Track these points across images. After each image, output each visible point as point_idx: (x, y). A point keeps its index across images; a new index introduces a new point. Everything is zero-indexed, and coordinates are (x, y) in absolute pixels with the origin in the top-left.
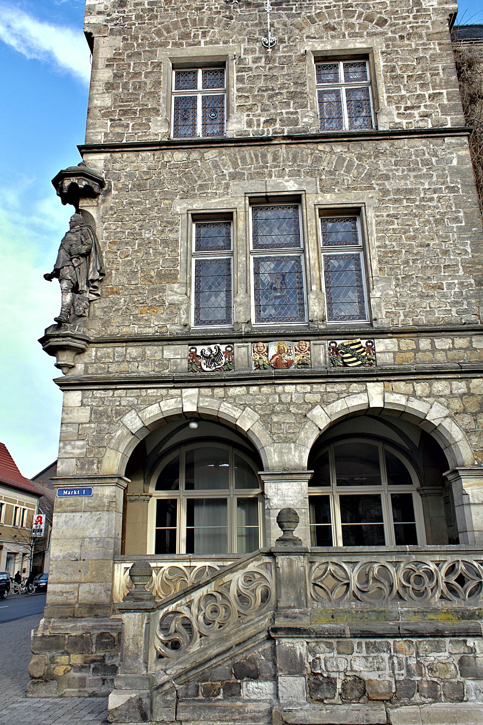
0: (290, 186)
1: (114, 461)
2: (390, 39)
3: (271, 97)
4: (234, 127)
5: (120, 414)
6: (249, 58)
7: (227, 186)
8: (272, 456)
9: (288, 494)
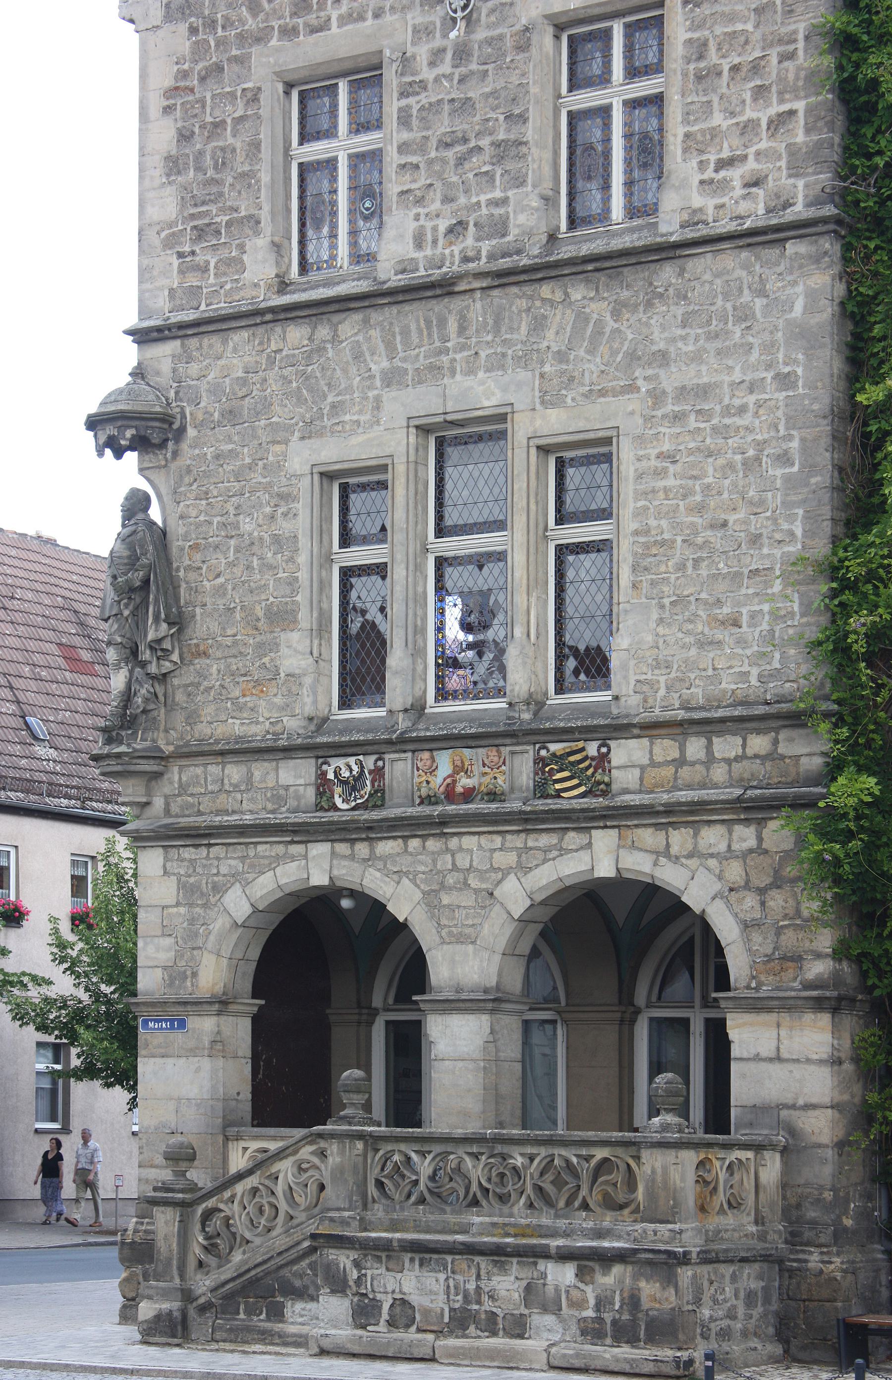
3: (461, 161)
4: (398, 248)
5: (219, 889)
6: (422, 52)
7: (378, 406)
8: (447, 967)
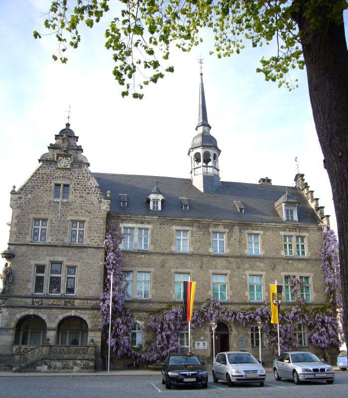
0: (60, 259)
1: (13, 325)
2: (91, 218)
3: (58, 232)
4: (49, 240)
6: (54, 220)
7: (45, 258)
8: (49, 325)
9: (51, 335)
